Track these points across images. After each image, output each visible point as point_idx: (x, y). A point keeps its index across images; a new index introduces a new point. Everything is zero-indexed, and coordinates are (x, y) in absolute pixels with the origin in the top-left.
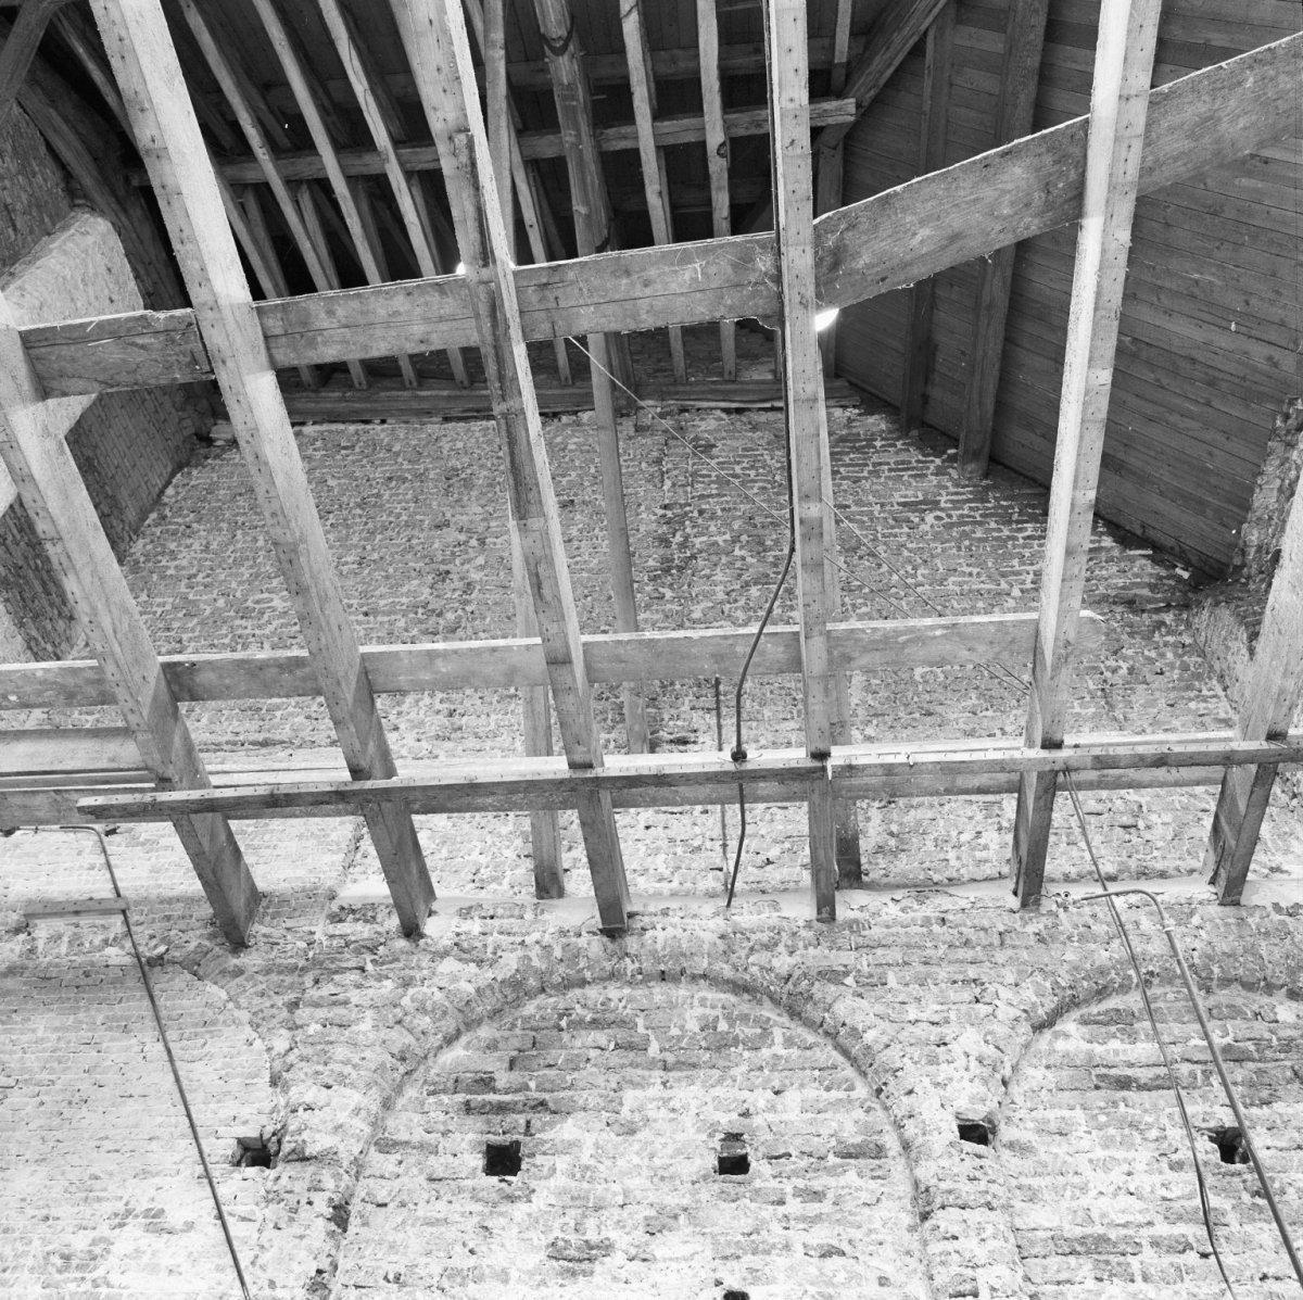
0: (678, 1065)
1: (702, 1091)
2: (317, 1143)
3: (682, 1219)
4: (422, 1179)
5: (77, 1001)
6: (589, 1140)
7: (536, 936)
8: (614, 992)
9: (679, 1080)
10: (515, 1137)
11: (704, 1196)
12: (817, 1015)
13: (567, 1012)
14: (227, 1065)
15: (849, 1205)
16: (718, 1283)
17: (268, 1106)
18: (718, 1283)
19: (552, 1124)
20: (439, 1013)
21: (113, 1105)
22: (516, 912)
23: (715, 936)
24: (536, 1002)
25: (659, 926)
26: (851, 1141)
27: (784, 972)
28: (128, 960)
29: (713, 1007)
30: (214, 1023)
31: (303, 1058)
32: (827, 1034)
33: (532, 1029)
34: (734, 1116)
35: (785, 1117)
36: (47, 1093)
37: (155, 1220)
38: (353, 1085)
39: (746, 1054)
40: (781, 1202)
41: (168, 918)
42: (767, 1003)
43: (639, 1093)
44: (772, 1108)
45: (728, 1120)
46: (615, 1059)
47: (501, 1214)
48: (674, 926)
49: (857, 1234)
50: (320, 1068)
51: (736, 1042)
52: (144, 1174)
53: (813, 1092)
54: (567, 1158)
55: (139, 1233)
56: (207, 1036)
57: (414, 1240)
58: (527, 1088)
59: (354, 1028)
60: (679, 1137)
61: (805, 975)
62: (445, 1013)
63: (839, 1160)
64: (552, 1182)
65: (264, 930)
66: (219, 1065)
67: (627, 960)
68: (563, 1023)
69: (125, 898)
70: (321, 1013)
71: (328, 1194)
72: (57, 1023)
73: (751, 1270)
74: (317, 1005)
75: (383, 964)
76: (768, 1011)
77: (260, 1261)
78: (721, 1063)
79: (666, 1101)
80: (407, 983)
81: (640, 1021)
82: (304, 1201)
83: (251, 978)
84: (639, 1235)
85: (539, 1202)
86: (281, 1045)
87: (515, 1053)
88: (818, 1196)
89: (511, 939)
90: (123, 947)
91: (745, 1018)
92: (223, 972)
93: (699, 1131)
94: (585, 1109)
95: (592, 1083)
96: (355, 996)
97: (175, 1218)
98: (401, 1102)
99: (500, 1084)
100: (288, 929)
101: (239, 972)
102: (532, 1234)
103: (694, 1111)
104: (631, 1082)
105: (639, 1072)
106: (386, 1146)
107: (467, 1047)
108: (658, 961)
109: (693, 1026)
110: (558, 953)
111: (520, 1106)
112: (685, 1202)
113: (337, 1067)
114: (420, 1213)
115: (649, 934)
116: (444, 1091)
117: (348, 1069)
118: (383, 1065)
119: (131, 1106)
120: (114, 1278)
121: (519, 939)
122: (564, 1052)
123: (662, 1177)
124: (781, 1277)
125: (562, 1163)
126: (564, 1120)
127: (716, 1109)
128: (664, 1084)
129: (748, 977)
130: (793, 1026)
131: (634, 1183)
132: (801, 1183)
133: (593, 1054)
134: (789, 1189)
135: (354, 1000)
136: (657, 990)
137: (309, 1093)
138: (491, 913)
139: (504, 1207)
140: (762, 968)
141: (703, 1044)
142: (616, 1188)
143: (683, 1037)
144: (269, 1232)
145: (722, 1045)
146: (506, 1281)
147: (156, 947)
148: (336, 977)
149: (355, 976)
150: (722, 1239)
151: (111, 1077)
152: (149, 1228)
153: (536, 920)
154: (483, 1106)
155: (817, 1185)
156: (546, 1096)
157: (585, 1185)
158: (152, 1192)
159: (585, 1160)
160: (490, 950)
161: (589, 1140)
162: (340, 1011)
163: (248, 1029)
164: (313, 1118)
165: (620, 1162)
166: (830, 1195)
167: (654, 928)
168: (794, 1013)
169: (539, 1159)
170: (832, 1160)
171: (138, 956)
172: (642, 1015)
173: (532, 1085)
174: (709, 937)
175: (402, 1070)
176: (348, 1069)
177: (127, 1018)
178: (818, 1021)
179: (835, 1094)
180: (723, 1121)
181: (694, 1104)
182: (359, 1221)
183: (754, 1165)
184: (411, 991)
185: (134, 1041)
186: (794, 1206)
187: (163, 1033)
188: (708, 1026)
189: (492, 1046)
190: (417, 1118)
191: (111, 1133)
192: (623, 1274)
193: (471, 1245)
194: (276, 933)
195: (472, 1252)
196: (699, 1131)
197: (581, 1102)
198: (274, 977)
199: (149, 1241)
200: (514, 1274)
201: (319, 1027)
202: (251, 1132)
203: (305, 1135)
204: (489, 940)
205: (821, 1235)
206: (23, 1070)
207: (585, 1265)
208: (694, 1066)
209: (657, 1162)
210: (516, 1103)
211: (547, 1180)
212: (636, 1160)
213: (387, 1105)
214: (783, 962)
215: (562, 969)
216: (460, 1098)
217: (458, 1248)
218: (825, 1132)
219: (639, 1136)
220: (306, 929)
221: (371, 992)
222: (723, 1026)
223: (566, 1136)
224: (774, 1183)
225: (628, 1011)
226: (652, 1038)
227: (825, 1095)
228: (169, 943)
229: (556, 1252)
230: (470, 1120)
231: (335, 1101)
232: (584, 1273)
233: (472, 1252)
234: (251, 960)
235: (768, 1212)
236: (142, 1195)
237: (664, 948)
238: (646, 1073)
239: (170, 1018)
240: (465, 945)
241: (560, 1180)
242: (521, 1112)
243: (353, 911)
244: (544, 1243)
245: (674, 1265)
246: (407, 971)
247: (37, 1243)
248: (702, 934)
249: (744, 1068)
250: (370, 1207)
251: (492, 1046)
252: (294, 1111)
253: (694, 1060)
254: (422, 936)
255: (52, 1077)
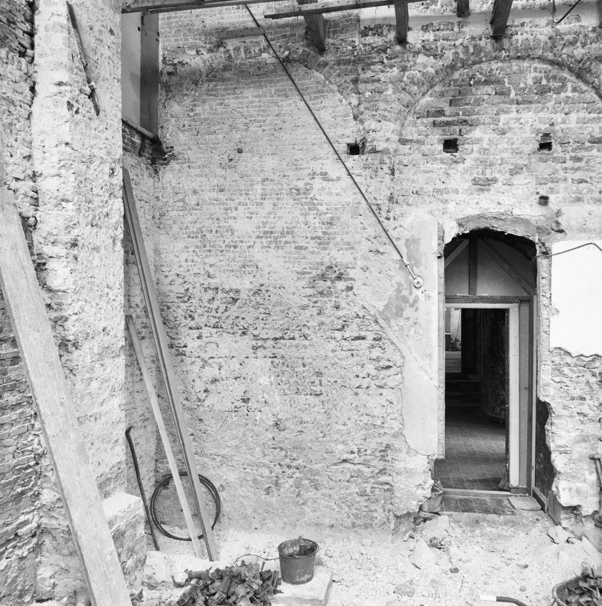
0: (523, 102)
1: (534, 115)
2: (381, 146)
3: (524, 169)
4: (420, 155)
5: (260, 83)
6: (486, 137)
7: (460, 41)
8: (494, 65)
9: (524, 109)
10: (455, 136)
11: (533, 160)
12: (591, 79)
13: (473, 77)
14: (334, 112)
15: (592, 163)
16: (538, 193)
17: (355, 129)
18: (538, 193)
19: (470, 131)
20: (421, 84)
21: (293, 130)
22: (450, 27)
23: (547, 37)
24: (459, 72)
25: (519, 33)
26: (597, 136)
27: (579, 58)
28: (274, 60)
29: (540, 72)
30: (323, 92)
31: (366, 108)
32: (593, 87)
33: (458, 86)
34: (547, 126)
35: (569, 126)
36: (264, 125)
37: (325, 176)
38: (389, 120)
39: (554, 96)
40: (564, 162)
41: (285, 36)
42: (566, 70)
43: (507, 116)
44: (564, 122)
45: (544, 127)
46: (497, 99)
47: (453, 169)
48: (527, 33)
49: (593, 174)
50: (374, 113)
51: (550, 90)
52: (315, 159)
53: (582, 114)
54: (478, 146)
55: (321, 181)
56: (322, 98)
57: (421, 179)
58: (458, 115)
59: (385, 93)
60: (523, 135)
61: (589, 59)
62: (423, 84)
63: (590, 144)
64: (472, 156)
65: (331, 41)
66: (330, 112)
67: (503, 52)
68: (472, 82)
69: (262, 27)
70: (370, 86)
71: (388, 165)
72: (256, 94)
73: (550, 188)
74: (366, 82)
75: (391, 59)
76: (566, 74)
77: (368, 191)
78: (543, 101)
79: (519, 119)
80: (404, 69)
81: (506, 80)
82: (379, 168)
83: (332, 68)
84: (507, 176)
85: (468, 163)
86: (355, 102)
87: (451, 98)
88: (579, 159)
89: (449, 43)
90: (269, 53)
91: (554, 77)
92: (319, 65)
93: (532, 133)
94: (484, 124)
95: (485, 113)
96: (382, 76)
97: (333, 175)
98: (407, 123)
99: (447, 113)
100: (342, 40)
101: (326, 64)
102: (466, 176)
103: (530, 124)
104: (503, 111)
105: (507, 106)
106: (403, 142)
107: (431, 96)
108: (518, 51)
109: (530, 82)
110: (471, 50)
111: (456, 122)
112: (525, 163)
113: (382, 112)
114: (422, 169)
115: (515, 37)
116: (423, 117)
117: (386, 113)
118: (401, 110)
119: (300, 131)
120: (317, 197)
121: (453, 43)
122: (473, 97)
123: (517, 152)
124: (562, 191)
125: (476, 147)
126: (475, 129)
127: (540, 123)
128: (517, 111)
129: (560, 59)
130: (577, 81)
131: (505, 155)
132: (573, 154)
133: (486, 97)
134: (568, 157)
135: (382, 79)
136: (514, 63)
137: (371, 124)
138: (437, 28)
139: (454, 166)
140: (568, 56)
141: (535, 91)
142: (498, 157)
143: (526, 88)
144: (369, 180)
145: (543, 91)
146: (458, 193)
147: (284, 52)
148: (372, 67)
149: (378, 67)
150: (540, 177)
151: (287, 118)
152: (324, 179)
153: (460, 32)
154: (441, 123)
155: (580, 155)
156: (467, 118)
157: (486, 157)
158: (321, 166)
159: (485, 146)
160: (439, 49)
161: (486, 137)
162: (376, 85)
163: (338, 95)
164: (377, 135)
165: (499, 147)
166: (585, 160)
167: (517, 34)
168: (579, 76)
169: (466, 146)
170: (587, 144)
171: (277, 57)
172: (507, 77)
173: (461, 113)
174: (543, 38)
175: (407, 111)
176: (386, 113)
177: (285, 90)
178: (591, 82)
179: (593, 115)
180: (543, 128)
181: (530, 120)
182: (398, 172)
183: (554, 146)
184: (407, 73)
185: (291, 101)
186: (569, 164)
187: (302, 96)
188: (537, 81)
189: (442, 95)
190: (414, 129)
191: (297, 142)
192: (502, 190)
193: (443, 180)
194: (337, 42)
195: (443, 182)
196: (532, 133)
197: (482, 121)
198: (343, 67)
199: (325, 184)
200: (460, 191)
201: (370, 93)
202: (351, 141)
203: (375, 143)
204: (439, 43)
205: (579, 175)
206: (251, 116)
207: (487, 187)
208: (531, 102)
209: (514, 146)
210: (454, 121)
211: (470, 154)
212: (506, 146)
213: (403, 125)
214: (579, 52)
215: (472, 58)
216: (431, 120)
217: (438, 181)
218: (586, 132)
219: (506, 135)
220: (350, 39)
221: (389, 74)
222: (544, 82)
223: (477, 136)
224: (562, 155)
225: (501, 75)
226: (512, 89)
227: (588, 116)
228: (289, 50)
229: (475, 182)
230: (436, 130)
231: (384, 128)
232: (487, 190)
233: (443, 182)
234: (329, 57)
235: (558, 166)
236: (317, 166)
237: (521, 45)
238: (509, 106)
239: (303, 90)
240: (428, 47)
241: (475, 155)
242: (456, 125)
243: (371, 29)
244: (470, 179)
245: (521, 187)
246: (403, 63)
247: (285, 185)
248: (539, 36)
249: (552, 103)
250: (401, 166)
251: (442, 95)
252: (368, 132)
253: (531, 99)
254: (407, 43)
255: (264, 119)
